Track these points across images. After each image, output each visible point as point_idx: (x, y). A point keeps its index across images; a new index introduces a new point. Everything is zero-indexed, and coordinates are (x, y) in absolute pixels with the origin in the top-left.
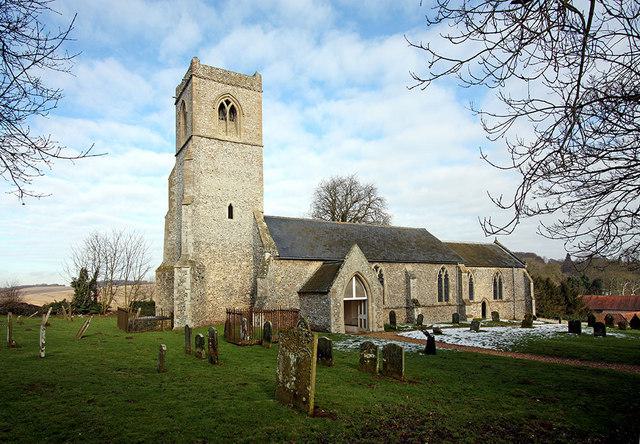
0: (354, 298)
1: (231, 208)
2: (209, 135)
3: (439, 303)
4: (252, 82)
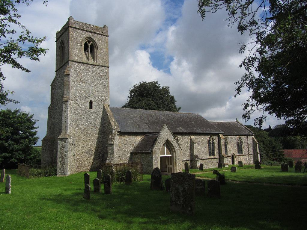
0: (166, 155)
1: (91, 103)
2: (78, 60)
3: (209, 157)
4: (103, 31)
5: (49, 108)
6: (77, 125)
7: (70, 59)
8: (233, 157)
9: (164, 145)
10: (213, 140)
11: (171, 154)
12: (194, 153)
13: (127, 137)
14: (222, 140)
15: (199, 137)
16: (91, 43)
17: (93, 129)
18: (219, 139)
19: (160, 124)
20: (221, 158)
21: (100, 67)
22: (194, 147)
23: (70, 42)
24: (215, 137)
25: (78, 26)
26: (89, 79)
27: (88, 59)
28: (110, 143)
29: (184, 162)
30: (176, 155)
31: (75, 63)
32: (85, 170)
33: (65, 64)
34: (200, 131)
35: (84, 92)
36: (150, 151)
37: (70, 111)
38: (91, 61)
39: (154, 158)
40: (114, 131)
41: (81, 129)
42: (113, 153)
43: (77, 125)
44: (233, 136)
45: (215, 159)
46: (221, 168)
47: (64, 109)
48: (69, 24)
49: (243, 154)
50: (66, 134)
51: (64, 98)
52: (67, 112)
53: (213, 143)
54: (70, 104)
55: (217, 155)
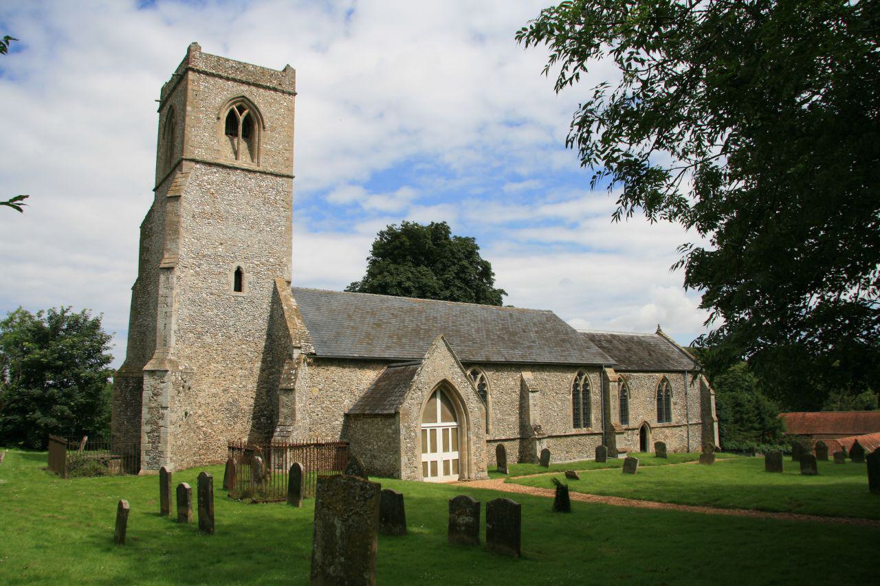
1: (239, 274)
2: (209, 158)
3: (574, 431)
5: (134, 288)
6: (199, 336)
7: (187, 155)
8: (643, 431)
9: (434, 395)
10: (484, 385)
11: (456, 421)
12: (529, 419)
13: (335, 372)
14: (610, 383)
15: (545, 375)
16: (246, 112)
17: (244, 346)
18: (605, 381)
19: (424, 336)
20: (608, 433)
21: (269, 176)
22: (531, 402)
23: (189, 108)
24: (591, 376)
25: (213, 68)
26: (235, 209)
27: (236, 153)
28: (284, 386)
29: (496, 444)
30: (468, 423)
31: (198, 166)
32: (219, 459)
33: (174, 170)
34: (546, 358)
35: (221, 244)
36: (393, 412)
37: (178, 294)
38: (244, 161)
39: (403, 431)
40: (296, 353)
41: (210, 345)
42: (292, 415)
43: (199, 336)
44: (645, 374)
45: (592, 437)
46: (604, 461)
47: (162, 291)
48: (188, 63)
49: (674, 422)
50: (162, 361)
51: (164, 261)
52: (169, 300)
53: (586, 392)
54: (179, 278)
55: (596, 425)
